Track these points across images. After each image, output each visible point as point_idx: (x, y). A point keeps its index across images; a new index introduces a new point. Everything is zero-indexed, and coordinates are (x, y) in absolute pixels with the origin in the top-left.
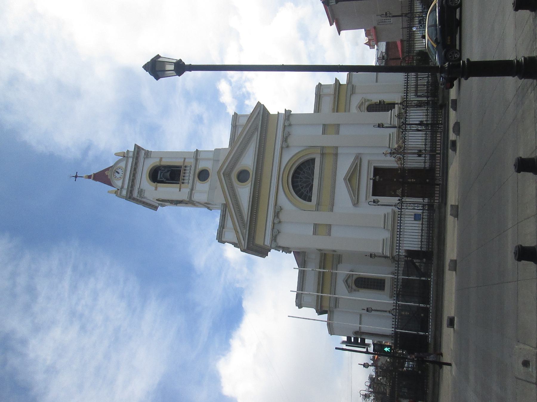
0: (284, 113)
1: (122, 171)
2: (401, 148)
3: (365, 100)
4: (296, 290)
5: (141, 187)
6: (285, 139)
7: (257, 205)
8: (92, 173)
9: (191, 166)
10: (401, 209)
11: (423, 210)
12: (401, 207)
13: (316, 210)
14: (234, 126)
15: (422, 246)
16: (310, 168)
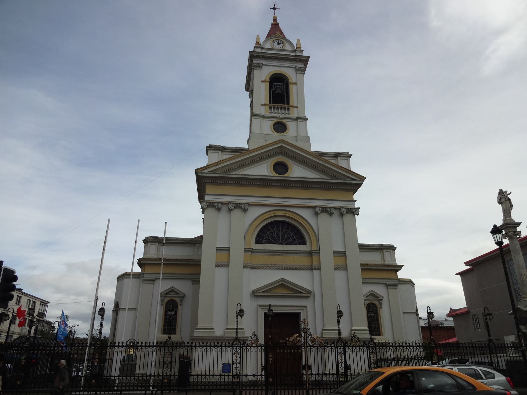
1: (280, 48)
3: (382, 300)
5: (263, 67)
6: (325, 210)
9: (290, 114)
10: (233, 346)
13: (245, 249)
14: (336, 155)
16: (294, 239)
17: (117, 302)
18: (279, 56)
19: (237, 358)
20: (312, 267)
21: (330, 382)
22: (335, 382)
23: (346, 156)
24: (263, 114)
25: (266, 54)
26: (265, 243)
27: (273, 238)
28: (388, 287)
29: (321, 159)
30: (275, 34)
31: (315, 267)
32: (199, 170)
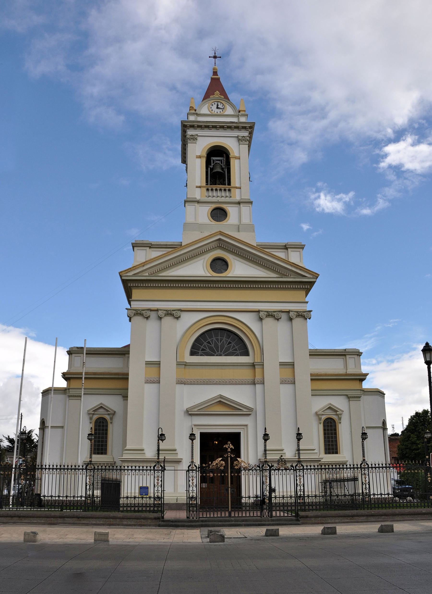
5: (199, 138)
6: (270, 315)
9: (231, 197)
10: (154, 470)
11: (154, 498)
12: (89, 469)
15: (347, 496)
17: (43, 419)
20: (254, 382)
21: (287, 504)
22: (317, 503)
26: (201, 355)
27: (211, 349)
28: (349, 399)
29: (262, 251)
30: (214, 95)
32: (123, 273)
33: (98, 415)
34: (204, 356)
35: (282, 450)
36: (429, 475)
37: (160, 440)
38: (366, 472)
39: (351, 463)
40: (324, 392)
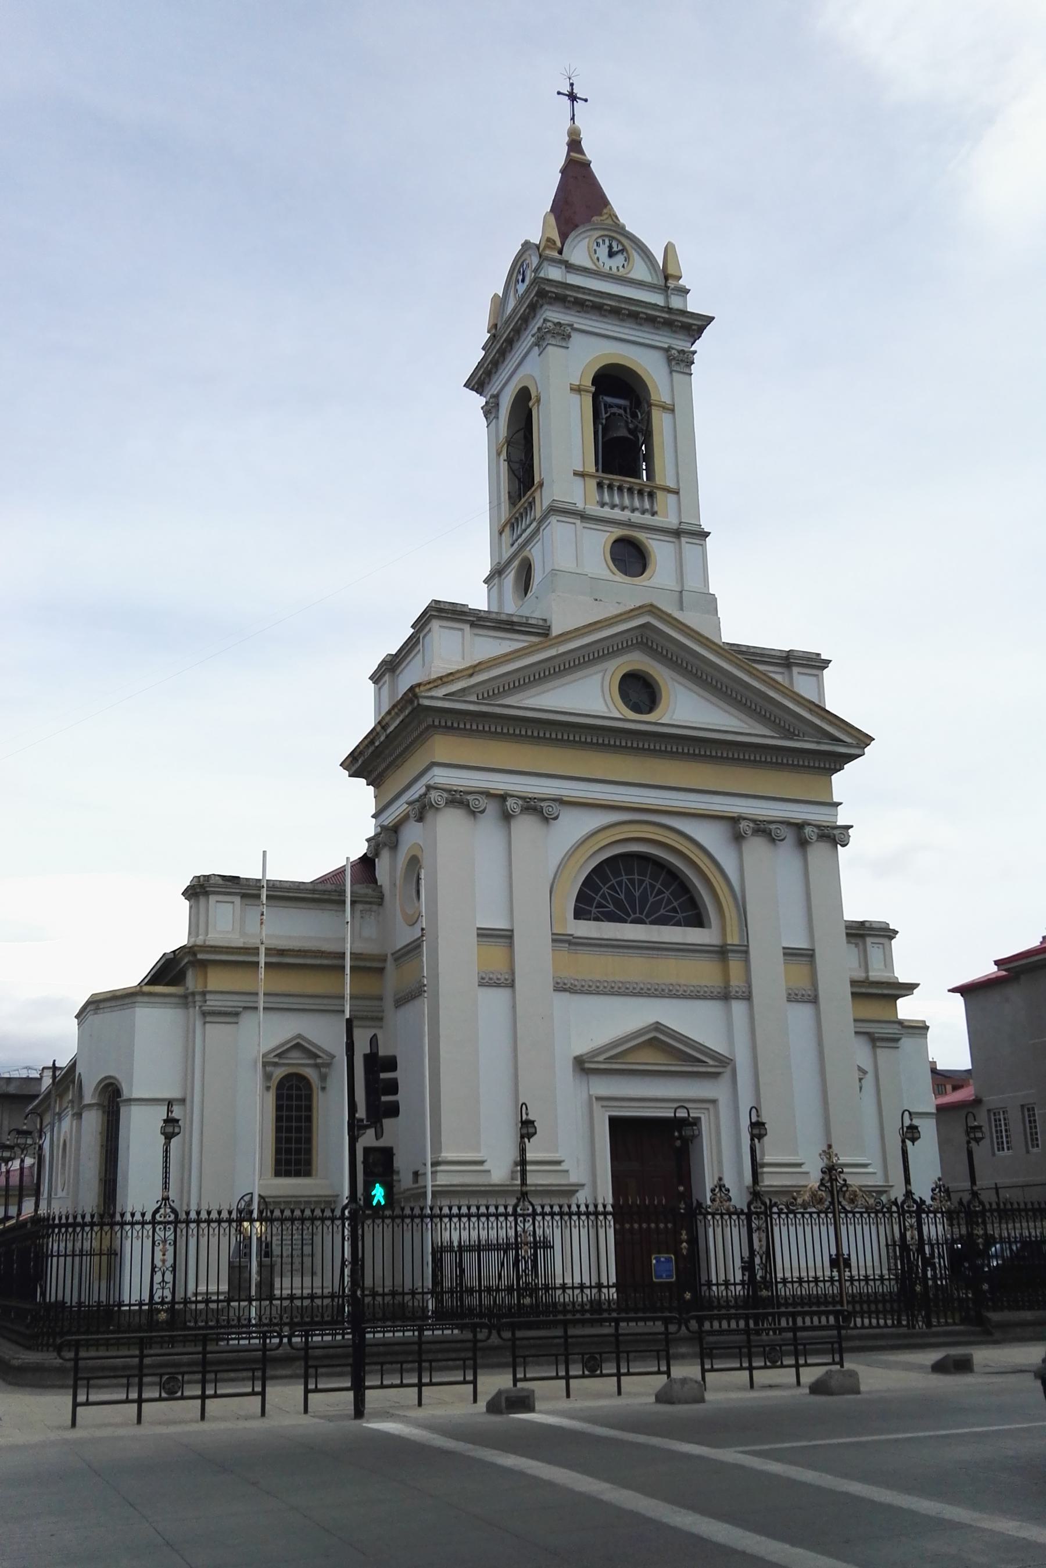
0: (839, 823)
2: (852, 1201)
4: (268, 878)
5: (576, 337)
6: (763, 829)
7: (592, 743)
8: (590, 150)
9: (654, 514)
10: (154, 1222)
14: (788, 660)
18: (623, 306)
19: (165, 1257)
23: (814, 664)
24: (580, 506)
25: (584, 293)
26: (597, 919)
29: (747, 667)
31: (737, 992)
32: (422, 688)
33: (287, 1068)
34: (602, 921)
35: (481, 1163)
36: (684, 1237)
37: (907, 1141)
38: (527, 1225)
39: (590, 1201)
40: (884, 1025)
